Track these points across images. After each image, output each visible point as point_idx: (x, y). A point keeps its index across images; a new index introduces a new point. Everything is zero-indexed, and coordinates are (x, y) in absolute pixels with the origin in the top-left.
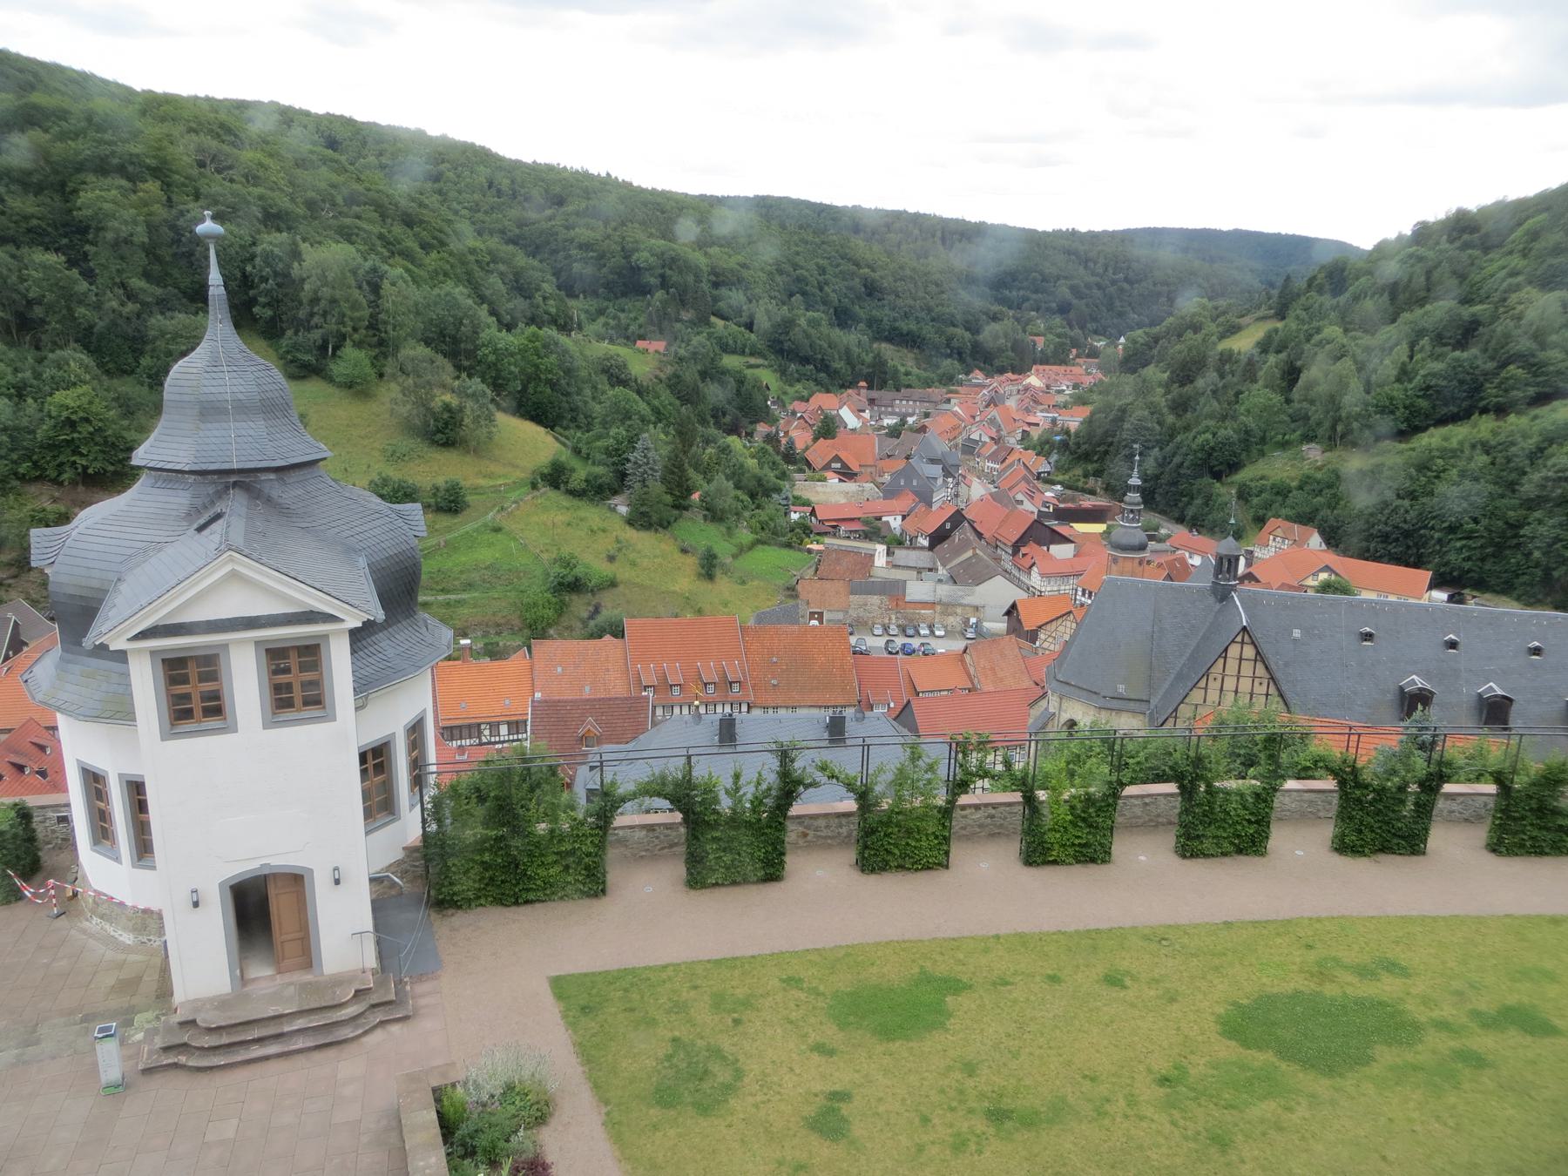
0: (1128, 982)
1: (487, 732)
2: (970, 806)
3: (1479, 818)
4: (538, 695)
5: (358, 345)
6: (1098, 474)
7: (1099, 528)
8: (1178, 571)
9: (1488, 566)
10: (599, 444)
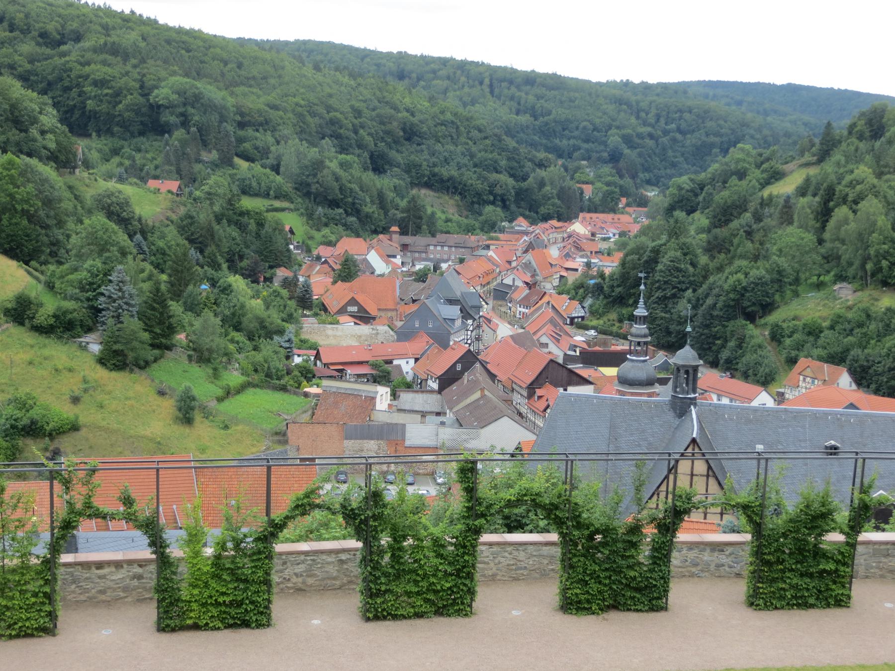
2: (109, 563)
10: (71, 277)
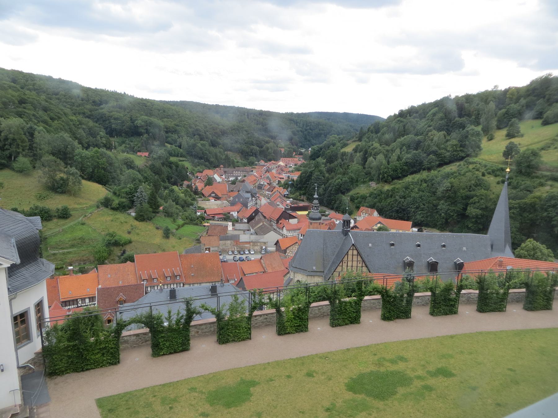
0: (315, 375)
1: (80, 302)
2: (258, 315)
3: (427, 304)
4: (100, 286)
5: (25, 156)
6: (304, 194)
7: (306, 213)
8: (332, 226)
9: (429, 219)
10: (123, 190)
